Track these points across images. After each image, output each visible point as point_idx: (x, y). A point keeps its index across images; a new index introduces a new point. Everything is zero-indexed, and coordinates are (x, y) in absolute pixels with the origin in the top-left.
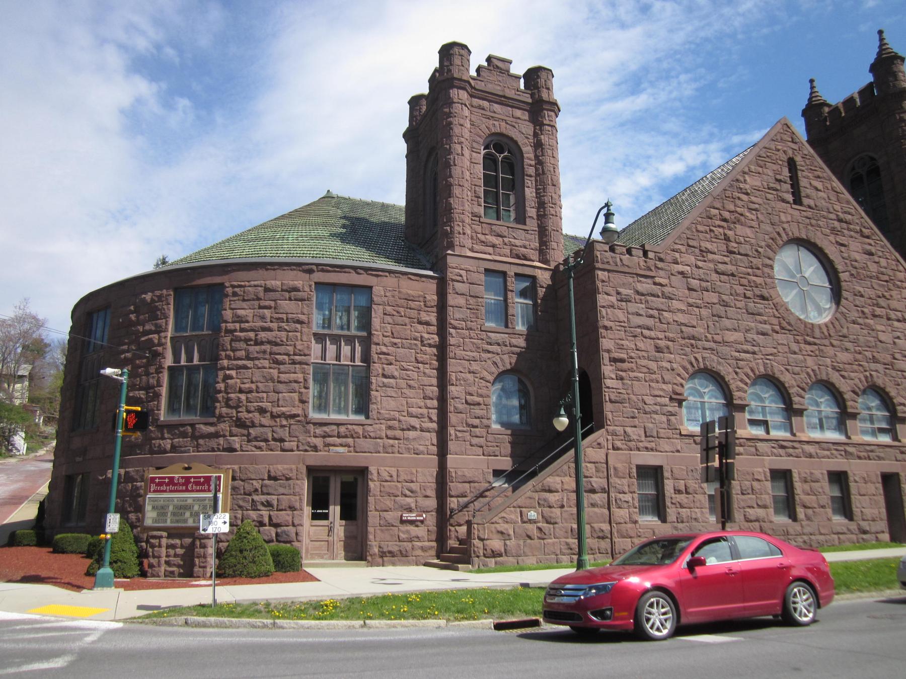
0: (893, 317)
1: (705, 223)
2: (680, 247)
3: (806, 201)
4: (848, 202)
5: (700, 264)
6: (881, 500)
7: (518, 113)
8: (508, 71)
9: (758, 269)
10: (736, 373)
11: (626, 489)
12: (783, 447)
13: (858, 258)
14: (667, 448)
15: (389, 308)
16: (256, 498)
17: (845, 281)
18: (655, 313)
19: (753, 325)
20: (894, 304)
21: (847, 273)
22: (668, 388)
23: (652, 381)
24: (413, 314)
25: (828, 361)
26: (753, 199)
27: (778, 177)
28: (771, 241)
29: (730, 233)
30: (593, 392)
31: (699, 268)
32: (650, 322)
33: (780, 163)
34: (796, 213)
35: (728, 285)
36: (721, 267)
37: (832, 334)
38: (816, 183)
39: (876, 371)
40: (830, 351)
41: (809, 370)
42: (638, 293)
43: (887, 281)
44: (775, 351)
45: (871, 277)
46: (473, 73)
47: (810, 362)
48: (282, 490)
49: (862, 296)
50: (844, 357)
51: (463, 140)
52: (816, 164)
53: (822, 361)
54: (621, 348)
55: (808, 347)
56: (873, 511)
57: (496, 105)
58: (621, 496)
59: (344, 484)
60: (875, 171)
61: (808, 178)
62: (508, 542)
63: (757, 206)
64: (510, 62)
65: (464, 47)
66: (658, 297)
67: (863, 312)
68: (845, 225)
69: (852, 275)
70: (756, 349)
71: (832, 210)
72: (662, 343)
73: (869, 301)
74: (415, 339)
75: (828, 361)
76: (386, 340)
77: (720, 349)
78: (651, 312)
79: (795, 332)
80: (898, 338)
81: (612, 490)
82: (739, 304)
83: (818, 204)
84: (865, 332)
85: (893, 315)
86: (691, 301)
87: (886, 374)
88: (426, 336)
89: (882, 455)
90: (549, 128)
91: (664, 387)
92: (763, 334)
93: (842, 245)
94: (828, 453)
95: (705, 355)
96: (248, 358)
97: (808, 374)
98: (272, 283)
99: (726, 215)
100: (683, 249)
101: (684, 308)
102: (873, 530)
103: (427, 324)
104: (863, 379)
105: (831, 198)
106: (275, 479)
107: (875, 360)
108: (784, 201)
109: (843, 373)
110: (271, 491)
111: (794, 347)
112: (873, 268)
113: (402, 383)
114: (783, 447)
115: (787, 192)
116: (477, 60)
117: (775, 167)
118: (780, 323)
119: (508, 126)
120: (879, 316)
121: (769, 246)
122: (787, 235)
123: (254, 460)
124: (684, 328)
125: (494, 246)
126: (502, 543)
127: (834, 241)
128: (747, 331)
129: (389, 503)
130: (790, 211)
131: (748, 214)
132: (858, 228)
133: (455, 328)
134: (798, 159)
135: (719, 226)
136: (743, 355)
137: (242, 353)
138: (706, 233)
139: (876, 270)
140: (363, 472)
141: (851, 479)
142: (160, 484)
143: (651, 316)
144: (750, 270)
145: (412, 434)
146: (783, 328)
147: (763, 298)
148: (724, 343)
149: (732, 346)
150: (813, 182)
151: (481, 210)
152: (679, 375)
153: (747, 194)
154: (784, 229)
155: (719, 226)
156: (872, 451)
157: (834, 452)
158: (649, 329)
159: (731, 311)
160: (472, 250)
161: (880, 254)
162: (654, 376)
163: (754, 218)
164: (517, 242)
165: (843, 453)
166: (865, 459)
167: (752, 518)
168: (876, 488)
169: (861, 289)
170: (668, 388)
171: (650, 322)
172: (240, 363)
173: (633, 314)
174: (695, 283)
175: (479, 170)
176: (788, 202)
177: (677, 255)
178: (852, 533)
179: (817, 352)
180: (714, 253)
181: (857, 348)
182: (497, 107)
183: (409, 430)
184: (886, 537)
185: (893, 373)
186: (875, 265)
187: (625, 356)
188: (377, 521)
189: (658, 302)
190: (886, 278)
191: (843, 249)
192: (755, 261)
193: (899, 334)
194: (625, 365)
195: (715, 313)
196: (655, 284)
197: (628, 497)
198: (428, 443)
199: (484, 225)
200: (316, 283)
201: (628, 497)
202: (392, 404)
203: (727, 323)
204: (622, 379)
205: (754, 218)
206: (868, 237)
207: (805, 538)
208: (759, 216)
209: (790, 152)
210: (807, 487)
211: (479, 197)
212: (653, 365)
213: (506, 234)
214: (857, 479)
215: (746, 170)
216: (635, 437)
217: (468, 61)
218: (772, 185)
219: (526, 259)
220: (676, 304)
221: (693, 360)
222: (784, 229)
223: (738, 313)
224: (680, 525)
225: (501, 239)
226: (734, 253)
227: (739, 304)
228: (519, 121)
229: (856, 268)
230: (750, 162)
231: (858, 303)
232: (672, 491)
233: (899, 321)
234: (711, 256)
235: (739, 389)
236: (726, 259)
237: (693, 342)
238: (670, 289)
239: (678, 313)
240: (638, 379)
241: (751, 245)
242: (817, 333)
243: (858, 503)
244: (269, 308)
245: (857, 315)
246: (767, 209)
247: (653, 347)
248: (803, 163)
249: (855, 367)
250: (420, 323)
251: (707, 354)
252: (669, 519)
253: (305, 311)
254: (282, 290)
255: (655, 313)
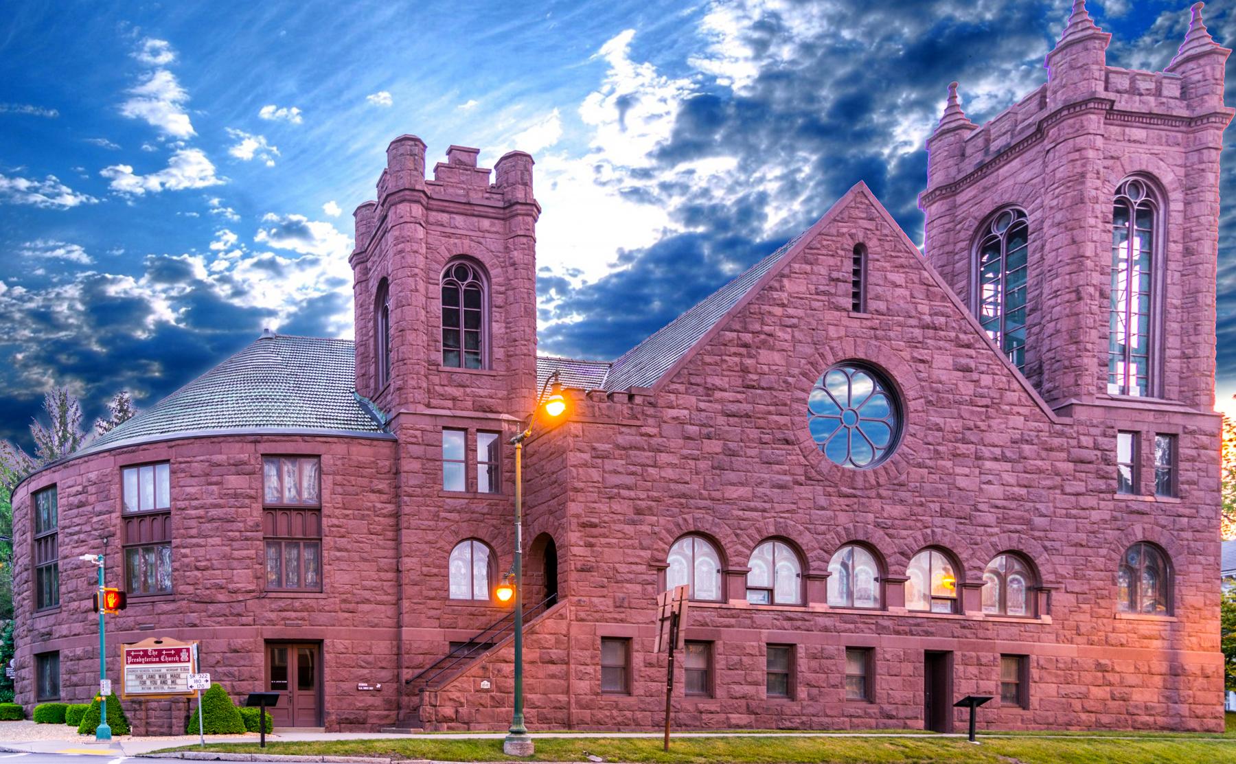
0: (987, 454)
1: (717, 352)
2: (678, 386)
3: (873, 305)
4: (945, 297)
5: (702, 405)
6: (921, 682)
7: (486, 223)
8: (474, 165)
9: (785, 405)
10: (737, 535)
11: (588, 661)
12: (790, 619)
13: (943, 378)
14: (641, 619)
15: (339, 478)
16: (219, 669)
17: (916, 411)
18: (638, 469)
19: (767, 476)
20: (992, 437)
21: (922, 400)
22: (647, 554)
23: (628, 547)
24: (365, 481)
25: (871, 516)
26: (791, 311)
27: (835, 275)
28: (809, 366)
29: (749, 362)
30: (559, 561)
31: (702, 410)
32: (629, 480)
33: (842, 253)
34: (856, 324)
35: (738, 430)
36: (734, 408)
37: (882, 481)
38: (893, 277)
39: (943, 527)
40: (876, 504)
41: (839, 529)
42: (618, 447)
43: (987, 406)
44: (794, 507)
45: (960, 403)
46: (430, 176)
47: (843, 518)
48: (242, 663)
49: (940, 429)
50: (898, 510)
51: (417, 270)
52: (901, 247)
53: (861, 516)
54: (593, 512)
55: (843, 501)
56: (905, 694)
57: (457, 217)
58: (582, 668)
59: (302, 658)
60: (1019, 234)
61: (884, 270)
62: (460, 709)
63: (795, 321)
64: (477, 152)
65: (416, 140)
66: (644, 450)
67: (936, 451)
68: (931, 332)
69: (929, 402)
70: (767, 506)
71: (913, 313)
72: (643, 504)
73: (951, 436)
74: (368, 509)
75: (871, 516)
76: (337, 512)
77: (717, 507)
78: (633, 468)
79: (827, 483)
80: (989, 483)
81: (572, 661)
82: (750, 452)
83: (894, 307)
84: (936, 477)
85: (986, 452)
86: (685, 452)
87: (958, 532)
88: (379, 505)
89: (932, 629)
90: (524, 240)
91: (642, 553)
92: (780, 487)
93: (922, 361)
94: (852, 626)
95: (697, 516)
96: (199, 536)
97: (837, 534)
98: (218, 458)
99: (747, 337)
100: (681, 388)
101: (676, 462)
102: (902, 714)
103: (380, 492)
104: (920, 537)
105: (916, 294)
106: (236, 651)
107: (943, 513)
108: (838, 308)
109: (891, 531)
110: (232, 662)
111: (822, 501)
112: (967, 389)
113: (356, 556)
114: (790, 619)
115: (846, 295)
116: (435, 157)
117: (831, 261)
118: (806, 472)
119: (473, 244)
120: (964, 456)
121: (805, 375)
122: (834, 354)
123: (215, 635)
124: (672, 486)
125: (454, 399)
126: (453, 710)
127: (908, 357)
128: (759, 484)
129: (344, 673)
130: (846, 321)
131: (780, 334)
132: (953, 334)
133: (410, 496)
134: (873, 245)
135: (735, 354)
136: (748, 514)
137: (194, 532)
138: (716, 364)
139: (971, 392)
140: (319, 643)
141: (879, 656)
142: (136, 657)
143: (633, 474)
144: (772, 408)
145: (366, 607)
146: (810, 479)
147: (787, 442)
148: (725, 500)
149: (734, 504)
150: (889, 276)
151: (439, 357)
152: (661, 539)
153: (783, 305)
154: (831, 348)
155: (735, 354)
156: (918, 625)
157: (862, 626)
158: (629, 488)
159: (738, 462)
160: (428, 406)
161: (984, 368)
162: (630, 542)
163: (788, 337)
164: (482, 392)
165: (873, 627)
166: (906, 634)
167: (738, 695)
168: (916, 672)
169: (940, 421)
170: (647, 554)
171: (629, 480)
172: (194, 541)
173: (610, 472)
174: (692, 430)
175: (437, 307)
176: (845, 310)
177: (673, 397)
178: (871, 717)
179: (856, 507)
180: (725, 390)
181: (918, 499)
182: (459, 220)
183: (363, 602)
184: (921, 723)
185: (970, 529)
186: (971, 386)
187: (596, 521)
188: (333, 690)
189: (645, 456)
190: (987, 401)
191: (921, 366)
192: (781, 395)
193: (990, 477)
194: (595, 531)
195: (716, 465)
196: (642, 435)
197: (590, 669)
198: (382, 616)
199: (443, 375)
200: (768, 644)
201: (590, 669)
202: (346, 578)
203: (732, 476)
204: (591, 545)
205: (788, 337)
206: (968, 346)
207: (804, 718)
208: (796, 334)
209: (860, 237)
210: (814, 664)
211: (437, 341)
212: (629, 529)
213: (468, 383)
214: (887, 656)
215: (786, 271)
216: (602, 608)
217: (423, 159)
218: (822, 288)
219: (492, 411)
220: (664, 458)
221: (681, 522)
222: (831, 348)
223: (747, 463)
224: (648, 699)
225: (462, 390)
226: (753, 387)
227: (750, 452)
228: (487, 235)
229: (938, 392)
230: (794, 260)
231: (930, 439)
232: (642, 664)
233: (996, 459)
234: (718, 394)
235: (739, 554)
236: (739, 396)
237: (683, 501)
238: (660, 440)
239: (668, 468)
240: (609, 545)
241: (779, 374)
242: (860, 482)
243: (883, 684)
244: (216, 484)
245: (925, 455)
246: (809, 323)
247: (631, 510)
248: (878, 249)
249: (912, 523)
250: (373, 491)
251: (699, 514)
252: (636, 692)
253: (253, 485)
254: (230, 465)
255: (638, 469)
